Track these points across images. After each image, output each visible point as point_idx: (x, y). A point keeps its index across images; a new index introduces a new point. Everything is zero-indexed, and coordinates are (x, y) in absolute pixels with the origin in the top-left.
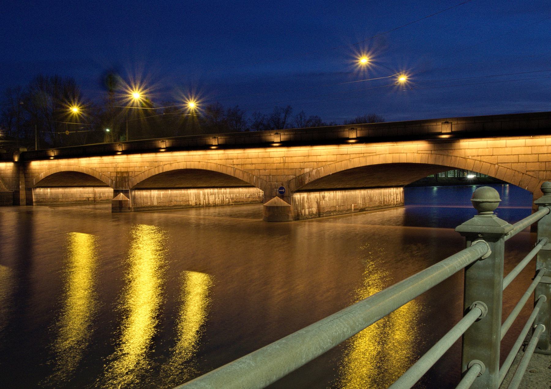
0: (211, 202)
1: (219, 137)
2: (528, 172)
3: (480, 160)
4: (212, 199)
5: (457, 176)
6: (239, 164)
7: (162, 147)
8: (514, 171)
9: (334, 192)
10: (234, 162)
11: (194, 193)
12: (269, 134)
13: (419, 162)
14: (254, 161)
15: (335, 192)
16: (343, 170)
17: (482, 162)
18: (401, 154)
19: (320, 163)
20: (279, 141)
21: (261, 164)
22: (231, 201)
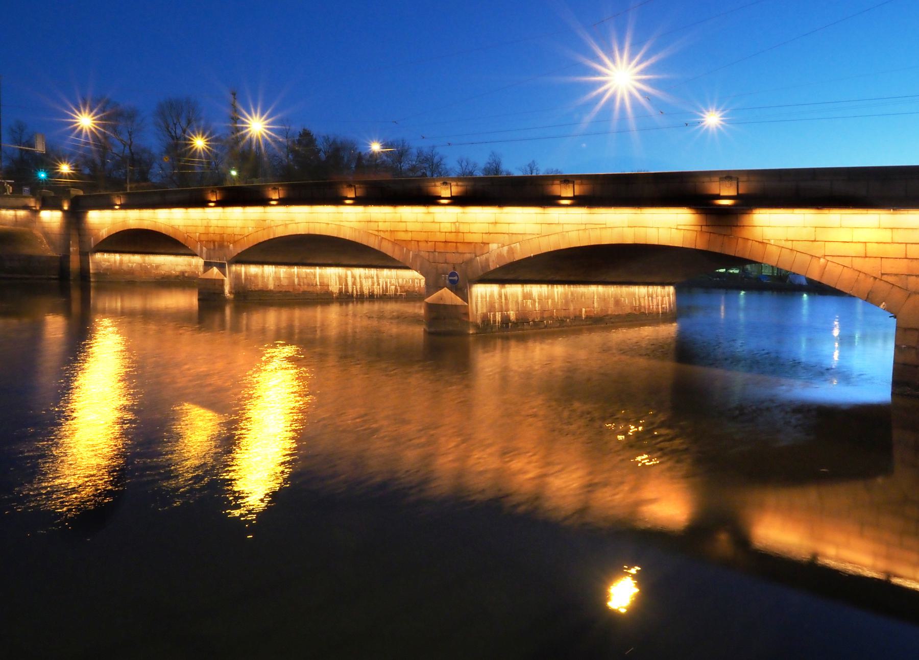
0: (366, 291)
1: (356, 186)
2: (885, 276)
3: (791, 248)
4: (367, 286)
5: (777, 274)
6: (387, 231)
7: (274, 198)
8: (857, 273)
9: (548, 287)
11: (337, 274)
12: (433, 184)
14: (411, 227)
15: (551, 287)
16: (552, 250)
17: (795, 252)
18: (648, 228)
19: (514, 235)
20: (450, 196)
21: (421, 232)
22: (399, 289)
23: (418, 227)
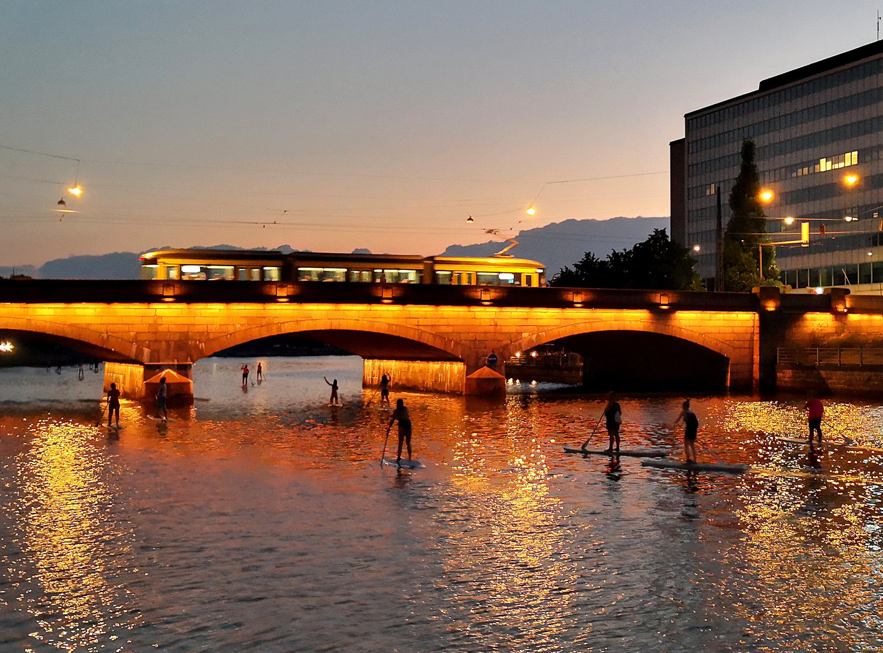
10: (420, 322)
13: (642, 330)
14: (452, 322)
20: (391, 297)
23: (460, 322)
